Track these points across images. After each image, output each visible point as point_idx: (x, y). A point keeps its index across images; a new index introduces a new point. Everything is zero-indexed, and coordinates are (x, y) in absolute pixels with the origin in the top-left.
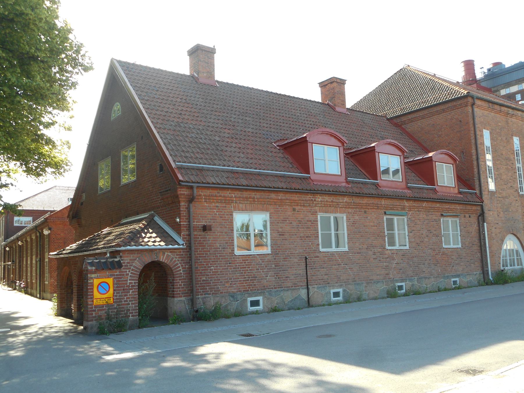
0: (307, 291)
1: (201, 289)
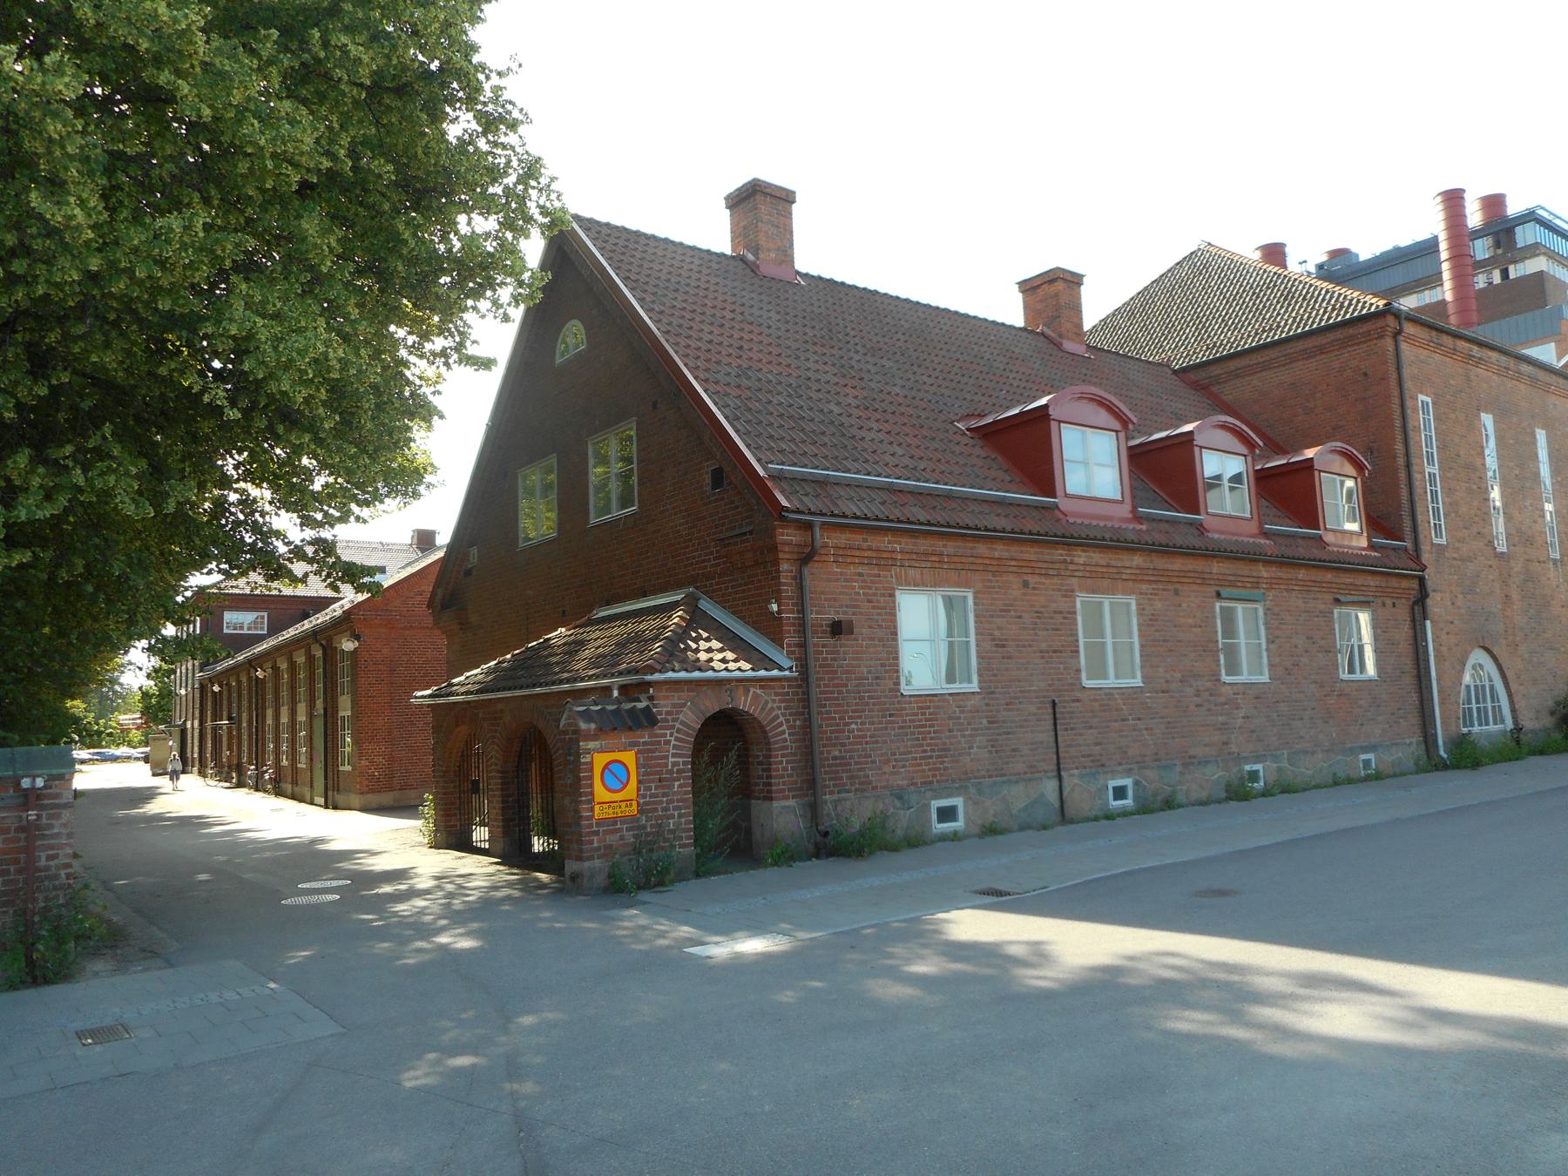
0: (1058, 783)
1: (830, 779)
